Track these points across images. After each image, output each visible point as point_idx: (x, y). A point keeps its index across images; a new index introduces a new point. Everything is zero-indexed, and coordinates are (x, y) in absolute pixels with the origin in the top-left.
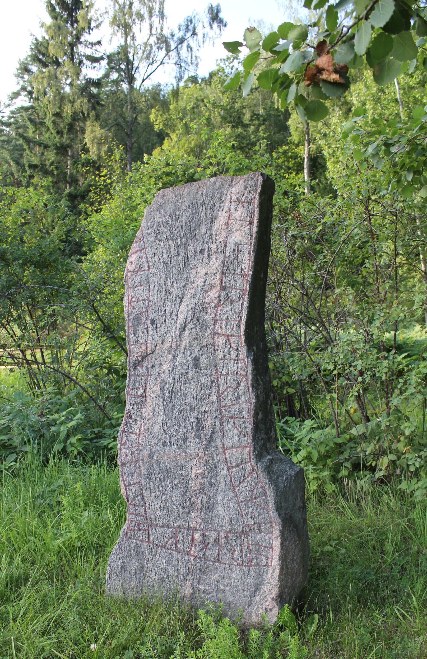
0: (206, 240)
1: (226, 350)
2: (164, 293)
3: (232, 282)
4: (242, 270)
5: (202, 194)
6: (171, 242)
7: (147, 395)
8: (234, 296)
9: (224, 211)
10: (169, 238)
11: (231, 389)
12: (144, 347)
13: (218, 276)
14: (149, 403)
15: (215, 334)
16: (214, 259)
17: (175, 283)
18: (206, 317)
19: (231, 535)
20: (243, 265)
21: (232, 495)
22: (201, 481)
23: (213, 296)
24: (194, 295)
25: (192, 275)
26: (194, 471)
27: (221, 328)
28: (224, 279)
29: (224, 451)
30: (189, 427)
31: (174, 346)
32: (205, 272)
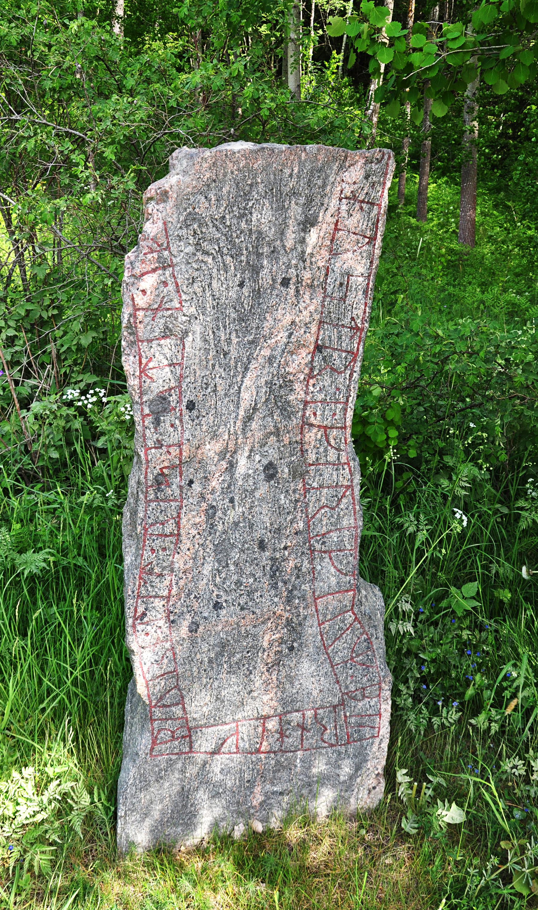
0: (294, 262)
1: (322, 450)
2: (212, 353)
3: (334, 337)
4: (353, 319)
5: (291, 175)
6: (228, 259)
7: (182, 531)
8: (338, 362)
9: (329, 214)
10: (225, 251)
11: (327, 509)
12: (174, 451)
13: (314, 328)
14: (186, 543)
15: (306, 424)
16: (307, 297)
18: (291, 398)
19: (321, 711)
20: (355, 312)
21: (323, 657)
22: (278, 649)
23: (303, 362)
24: (270, 360)
25: (266, 324)
26: (267, 637)
27: (315, 414)
28: (322, 332)
29: (315, 601)
30: (259, 574)
31: (231, 447)
32: (292, 317)
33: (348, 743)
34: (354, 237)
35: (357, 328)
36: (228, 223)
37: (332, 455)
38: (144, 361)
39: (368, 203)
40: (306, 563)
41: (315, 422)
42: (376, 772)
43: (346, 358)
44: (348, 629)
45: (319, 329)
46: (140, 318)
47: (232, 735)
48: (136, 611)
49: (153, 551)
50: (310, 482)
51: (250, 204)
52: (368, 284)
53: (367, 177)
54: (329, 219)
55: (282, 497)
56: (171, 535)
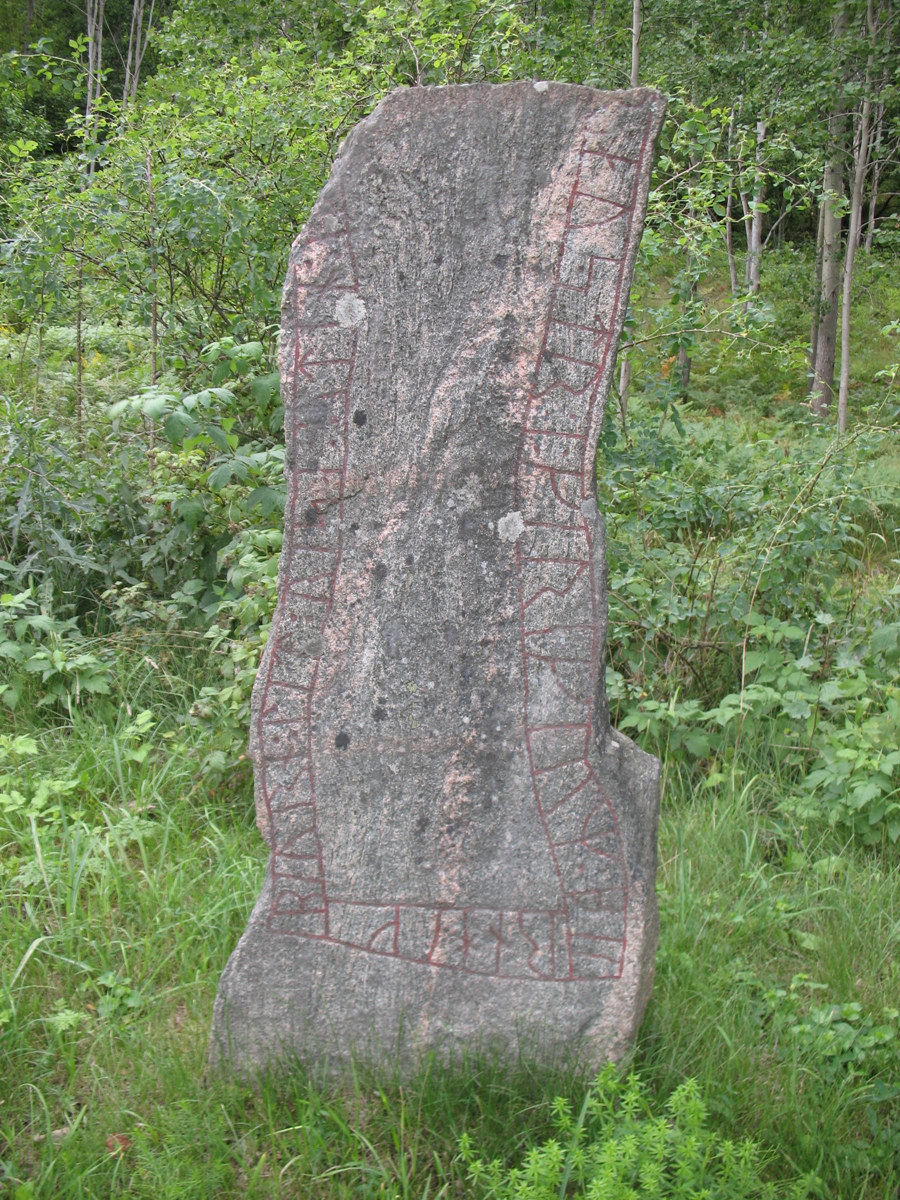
1: (546, 502)
4: (597, 318)
5: (512, 119)
10: (418, 215)
11: (550, 593)
16: (530, 285)
17: (424, 328)
19: (528, 916)
22: (466, 799)
26: (449, 779)
27: (537, 449)
28: (551, 334)
33: (570, 979)
34: (599, 204)
35: (603, 331)
36: (423, 179)
37: (562, 512)
38: (302, 352)
39: (622, 158)
40: (514, 670)
41: (537, 461)
42: (615, 1039)
43: (586, 373)
44: (578, 789)
45: (547, 329)
46: (302, 297)
47: (389, 924)
48: (264, 704)
49: (293, 616)
50: (527, 549)
51: (455, 154)
52: (621, 271)
53: (620, 125)
54: (563, 178)
55: (484, 565)
56: (321, 598)
